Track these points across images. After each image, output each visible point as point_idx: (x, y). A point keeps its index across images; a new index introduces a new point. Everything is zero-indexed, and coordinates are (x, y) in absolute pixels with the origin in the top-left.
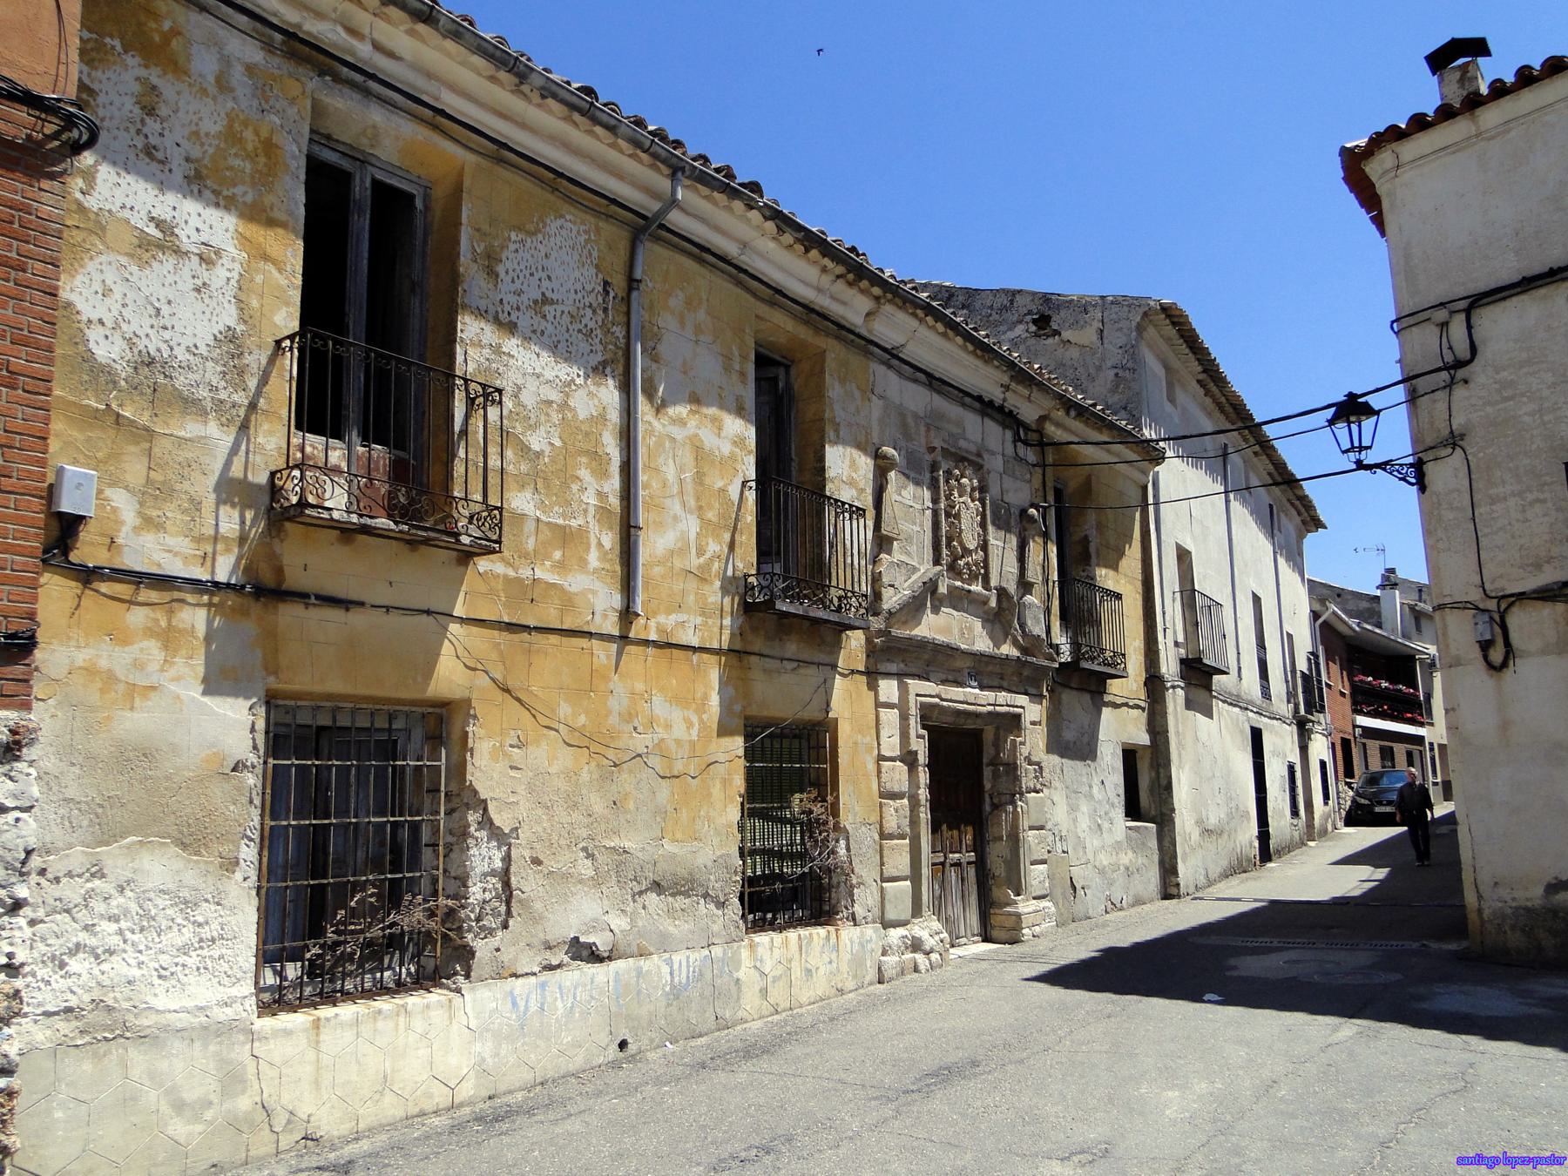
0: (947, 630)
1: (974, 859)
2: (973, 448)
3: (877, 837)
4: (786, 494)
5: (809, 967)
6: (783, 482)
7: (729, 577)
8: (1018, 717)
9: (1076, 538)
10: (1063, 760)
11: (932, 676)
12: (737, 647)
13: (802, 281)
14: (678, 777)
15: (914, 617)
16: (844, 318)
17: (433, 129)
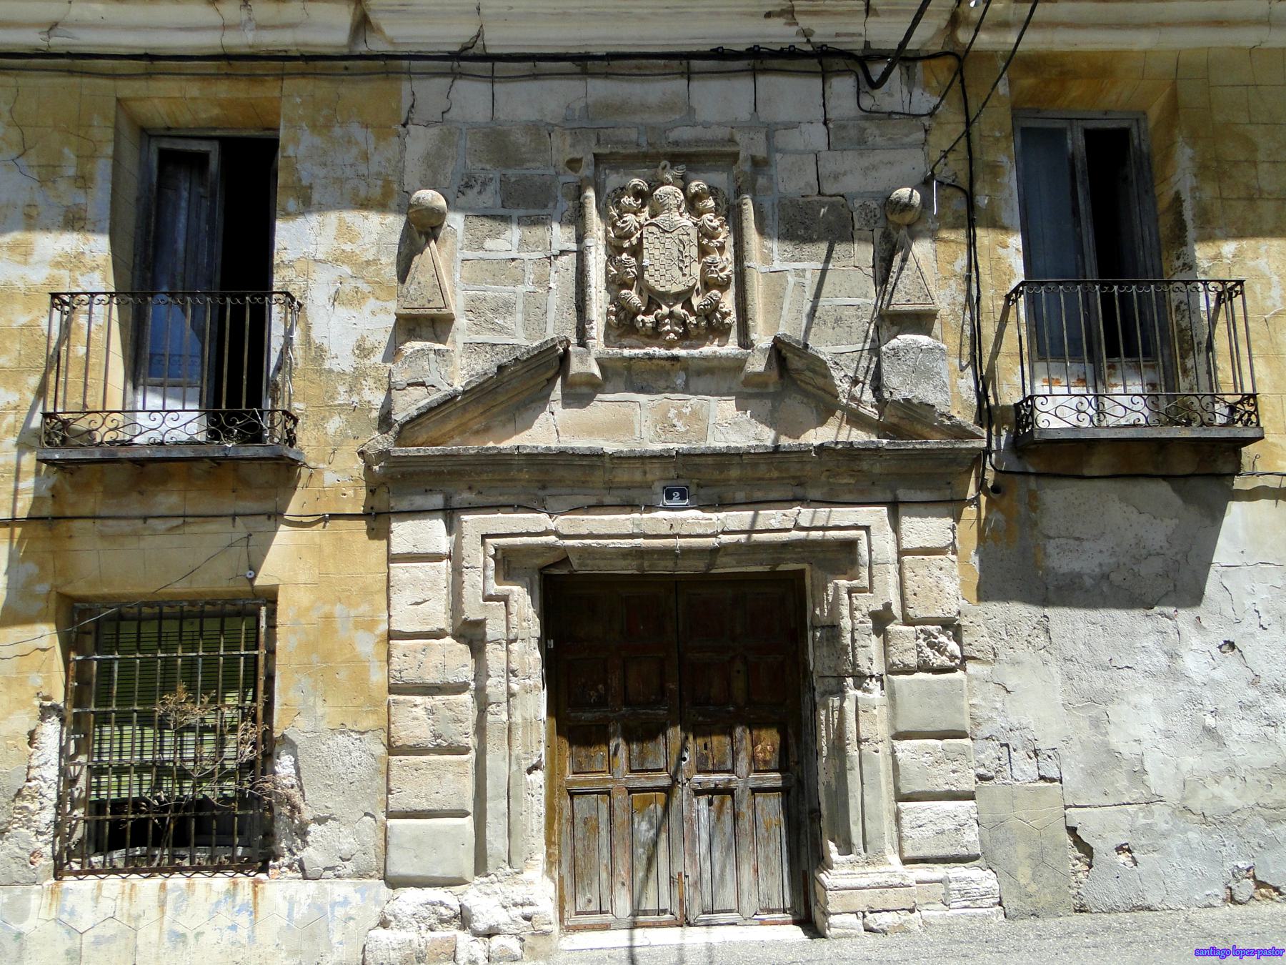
0: (625, 426)
1: (779, 784)
2: (722, 133)
3: (380, 750)
4: (1125, 298)
5: (180, 929)
6: (1134, 283)
7: (36, 430)
8: (851, 545)
9: (1164, 203)
10: (1047, 611)
11: (550, 502)
12: (47, 511)
13: (181, 29)
14: (388, 661)
15: (512, 419)
16: (306, 45)
17: (535, 79)
